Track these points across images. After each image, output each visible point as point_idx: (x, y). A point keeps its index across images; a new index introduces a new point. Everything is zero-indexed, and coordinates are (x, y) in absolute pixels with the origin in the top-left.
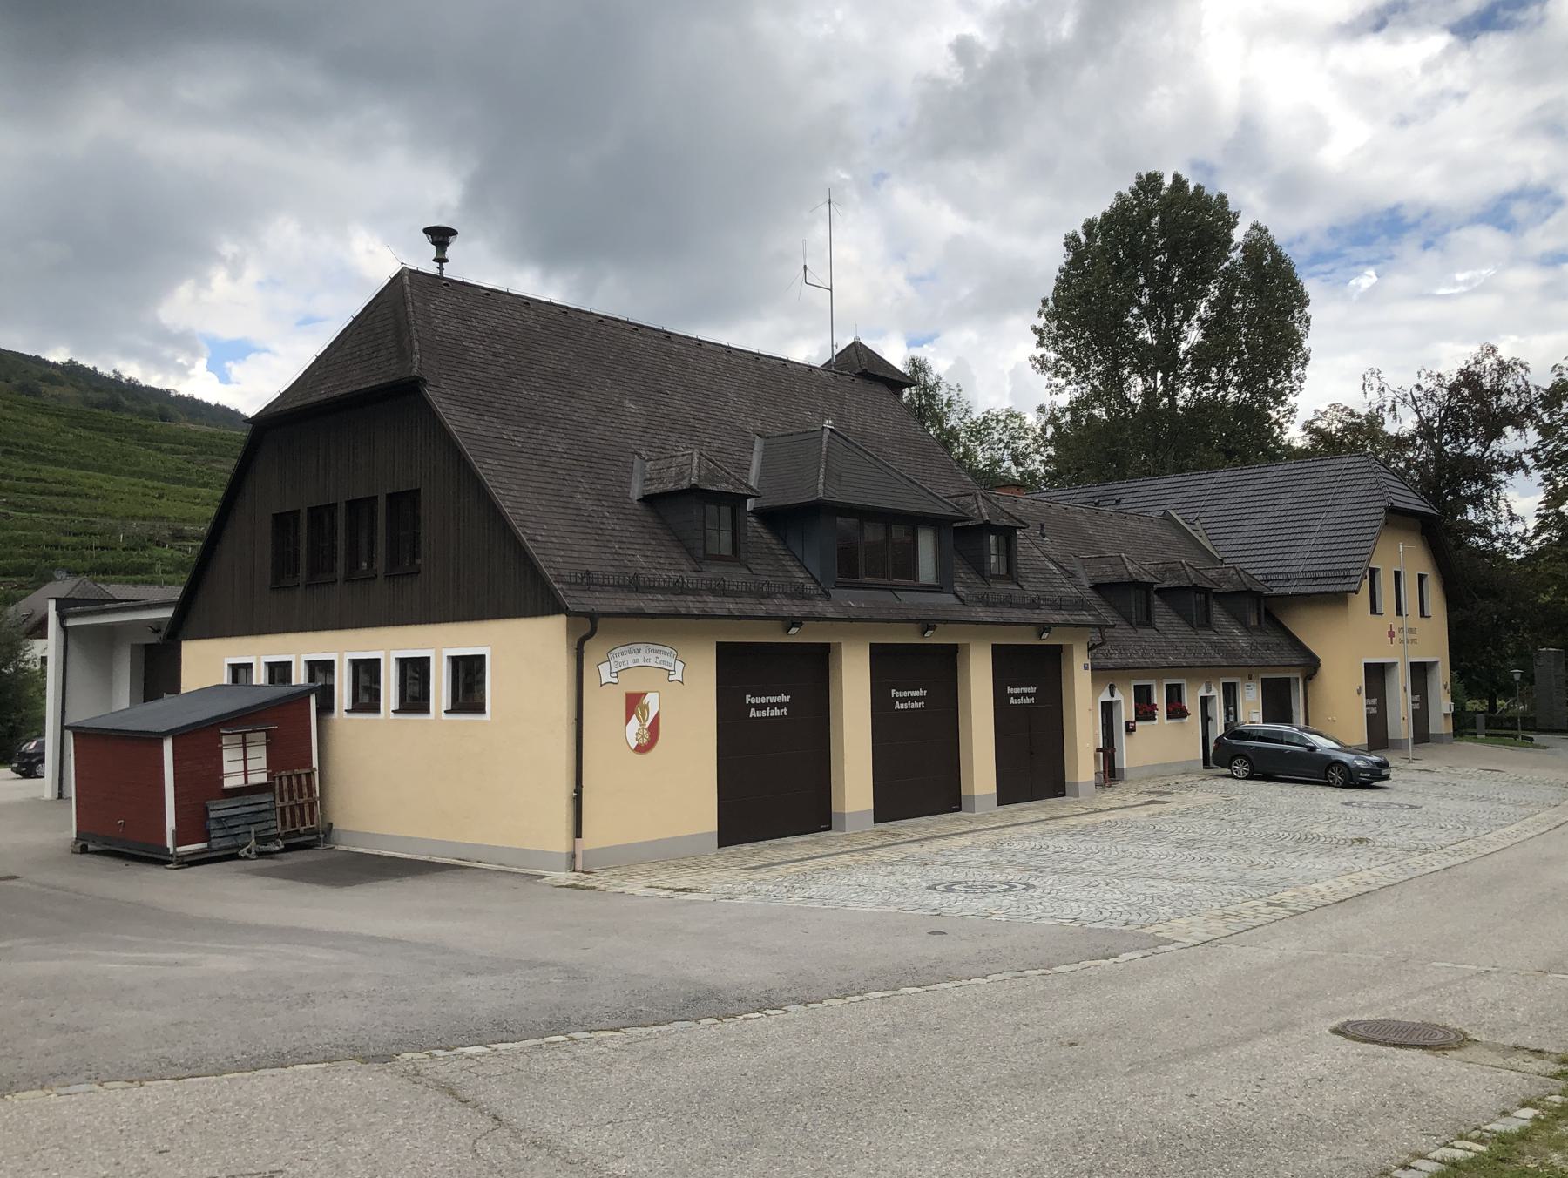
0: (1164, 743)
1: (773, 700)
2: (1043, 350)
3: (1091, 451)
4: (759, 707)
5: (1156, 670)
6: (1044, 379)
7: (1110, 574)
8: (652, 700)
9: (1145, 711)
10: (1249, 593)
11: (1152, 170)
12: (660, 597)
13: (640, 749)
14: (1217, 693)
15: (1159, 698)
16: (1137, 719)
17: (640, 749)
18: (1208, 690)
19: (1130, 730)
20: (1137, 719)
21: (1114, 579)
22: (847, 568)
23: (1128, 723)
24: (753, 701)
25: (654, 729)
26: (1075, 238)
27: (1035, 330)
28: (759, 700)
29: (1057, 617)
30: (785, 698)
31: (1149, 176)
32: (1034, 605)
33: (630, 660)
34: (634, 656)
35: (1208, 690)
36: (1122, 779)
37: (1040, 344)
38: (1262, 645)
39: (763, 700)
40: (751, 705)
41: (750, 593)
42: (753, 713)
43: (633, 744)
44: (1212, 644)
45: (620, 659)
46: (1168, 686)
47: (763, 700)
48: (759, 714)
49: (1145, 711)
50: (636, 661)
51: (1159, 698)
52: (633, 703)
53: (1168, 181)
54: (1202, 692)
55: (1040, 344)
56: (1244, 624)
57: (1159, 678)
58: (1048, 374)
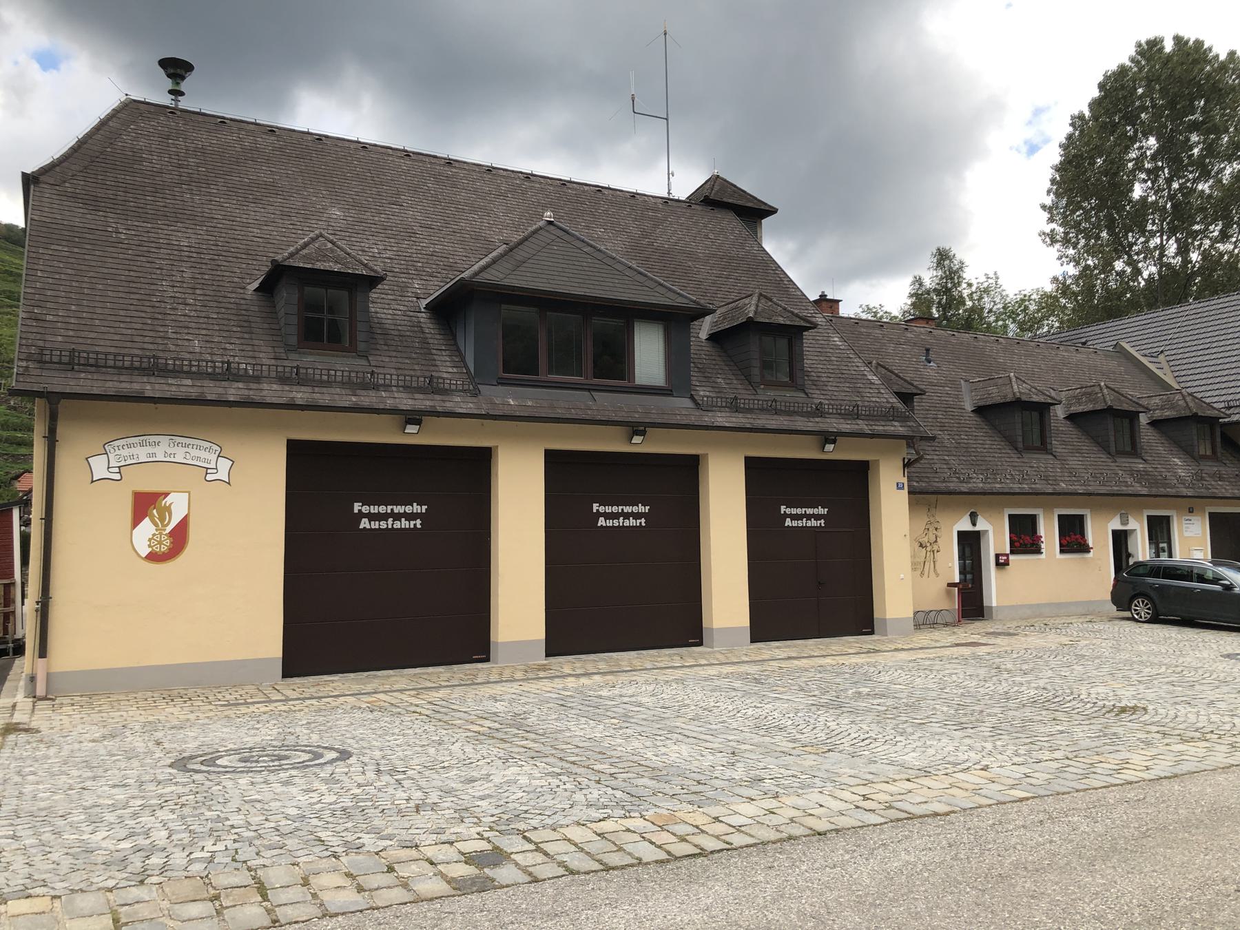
0: (1053, 583)
1: (810, 511)
2: (1053, 225)
3: (1091, 304)
4: (372, 517)
5: (1090, 498)
6: (1054, 251)
7: (995, 395)
8: (178, 506)
9: (1024, 538)
10: (1195, 418)
11: (1151, 36)
12: (189, 382)
13: (153, 557)
14: (1139, 528)
15: (1049, 531)
16: (1012, 552)
17: (153, 557)
18: (1124, 522)
19: (1001, 564)
20: (1012, 552)
21: (998, 400)
22: (519, 364)
23: (997, 556)
24: (788, 511)
25: (180, 536)
26: (1081, 117)
27: (1044, 207)
28: (794, 511)
29: (846, 426)
30: (821, 511)
31: (1148, 42)
32: (819, 412)
33: (142, 453)
34: (150, 450)
35: (1124, 522)
36: (991, 618)
37: (1051, 220)
38: (1213, 476)
39: (799, 511)
40: (786, 515)
41: (343, 384)
42: (788, 522)
43: (144, 551)
44: (1131, 472)
45: (126, 452)
46: (1210, 514)
47: (799, 511)
48: (795, 524)
49: (1024, 538)
50: (149, 455)
51: (1049, 531)
52: (144, 504)
53: (1169, 46)
54: (1115, 524)
55: (1051, 220)
56: (1189, 452)
57: (1048, 508)
58: (1057, 246)
